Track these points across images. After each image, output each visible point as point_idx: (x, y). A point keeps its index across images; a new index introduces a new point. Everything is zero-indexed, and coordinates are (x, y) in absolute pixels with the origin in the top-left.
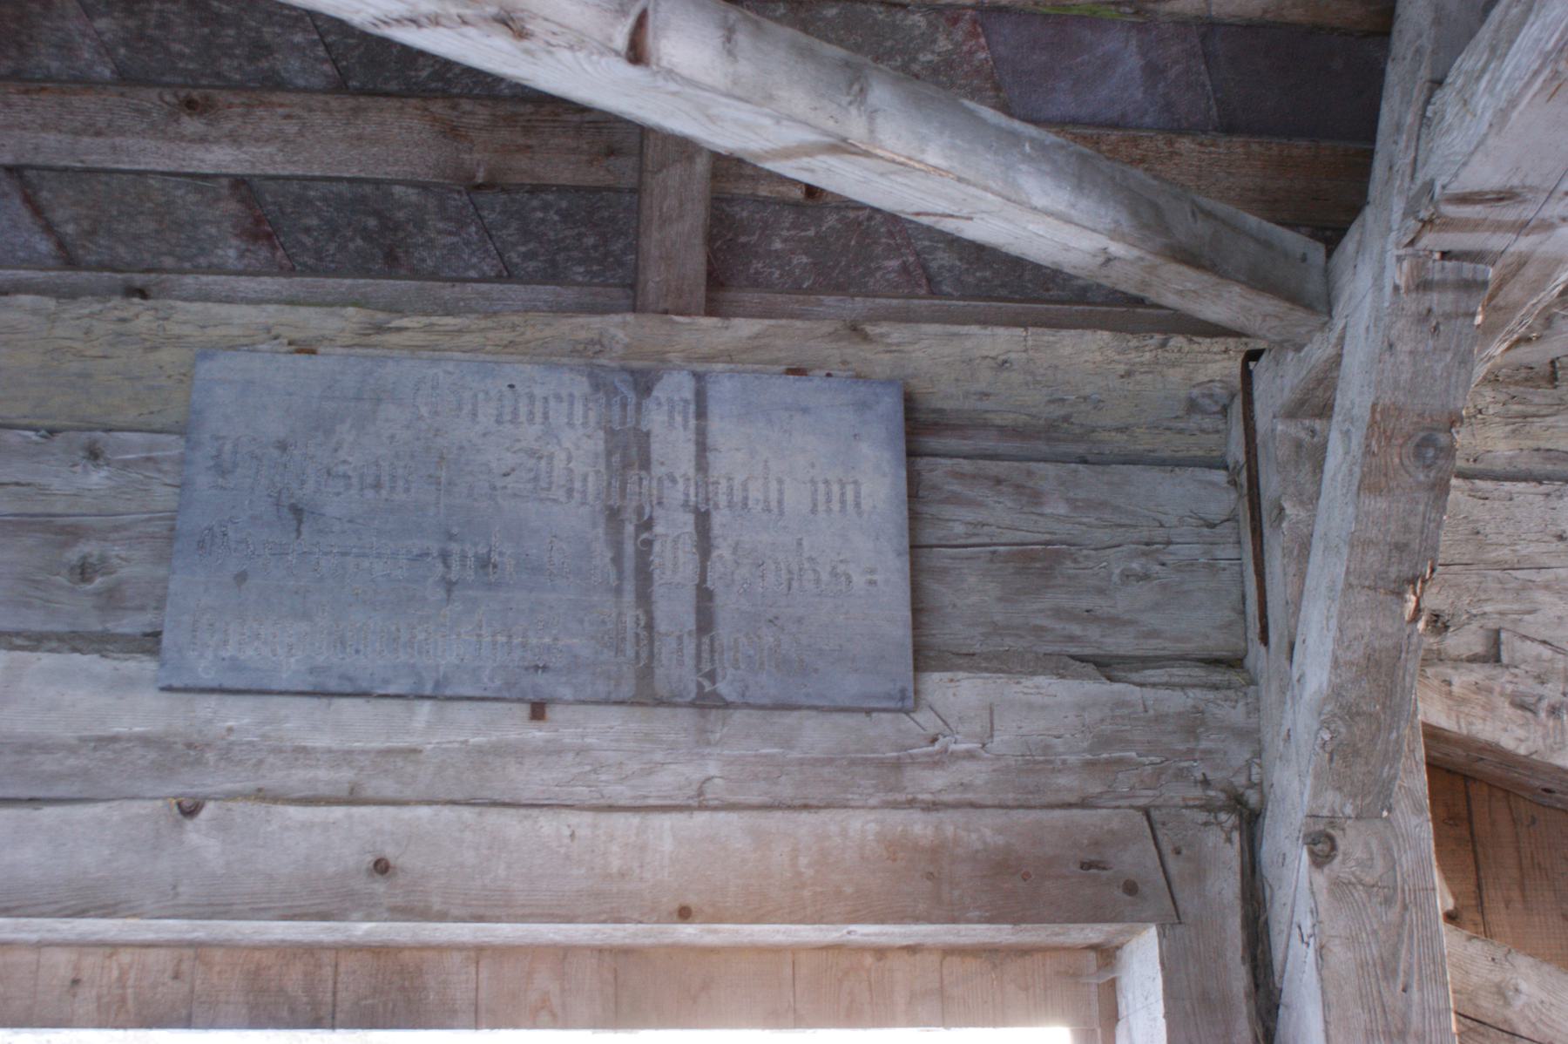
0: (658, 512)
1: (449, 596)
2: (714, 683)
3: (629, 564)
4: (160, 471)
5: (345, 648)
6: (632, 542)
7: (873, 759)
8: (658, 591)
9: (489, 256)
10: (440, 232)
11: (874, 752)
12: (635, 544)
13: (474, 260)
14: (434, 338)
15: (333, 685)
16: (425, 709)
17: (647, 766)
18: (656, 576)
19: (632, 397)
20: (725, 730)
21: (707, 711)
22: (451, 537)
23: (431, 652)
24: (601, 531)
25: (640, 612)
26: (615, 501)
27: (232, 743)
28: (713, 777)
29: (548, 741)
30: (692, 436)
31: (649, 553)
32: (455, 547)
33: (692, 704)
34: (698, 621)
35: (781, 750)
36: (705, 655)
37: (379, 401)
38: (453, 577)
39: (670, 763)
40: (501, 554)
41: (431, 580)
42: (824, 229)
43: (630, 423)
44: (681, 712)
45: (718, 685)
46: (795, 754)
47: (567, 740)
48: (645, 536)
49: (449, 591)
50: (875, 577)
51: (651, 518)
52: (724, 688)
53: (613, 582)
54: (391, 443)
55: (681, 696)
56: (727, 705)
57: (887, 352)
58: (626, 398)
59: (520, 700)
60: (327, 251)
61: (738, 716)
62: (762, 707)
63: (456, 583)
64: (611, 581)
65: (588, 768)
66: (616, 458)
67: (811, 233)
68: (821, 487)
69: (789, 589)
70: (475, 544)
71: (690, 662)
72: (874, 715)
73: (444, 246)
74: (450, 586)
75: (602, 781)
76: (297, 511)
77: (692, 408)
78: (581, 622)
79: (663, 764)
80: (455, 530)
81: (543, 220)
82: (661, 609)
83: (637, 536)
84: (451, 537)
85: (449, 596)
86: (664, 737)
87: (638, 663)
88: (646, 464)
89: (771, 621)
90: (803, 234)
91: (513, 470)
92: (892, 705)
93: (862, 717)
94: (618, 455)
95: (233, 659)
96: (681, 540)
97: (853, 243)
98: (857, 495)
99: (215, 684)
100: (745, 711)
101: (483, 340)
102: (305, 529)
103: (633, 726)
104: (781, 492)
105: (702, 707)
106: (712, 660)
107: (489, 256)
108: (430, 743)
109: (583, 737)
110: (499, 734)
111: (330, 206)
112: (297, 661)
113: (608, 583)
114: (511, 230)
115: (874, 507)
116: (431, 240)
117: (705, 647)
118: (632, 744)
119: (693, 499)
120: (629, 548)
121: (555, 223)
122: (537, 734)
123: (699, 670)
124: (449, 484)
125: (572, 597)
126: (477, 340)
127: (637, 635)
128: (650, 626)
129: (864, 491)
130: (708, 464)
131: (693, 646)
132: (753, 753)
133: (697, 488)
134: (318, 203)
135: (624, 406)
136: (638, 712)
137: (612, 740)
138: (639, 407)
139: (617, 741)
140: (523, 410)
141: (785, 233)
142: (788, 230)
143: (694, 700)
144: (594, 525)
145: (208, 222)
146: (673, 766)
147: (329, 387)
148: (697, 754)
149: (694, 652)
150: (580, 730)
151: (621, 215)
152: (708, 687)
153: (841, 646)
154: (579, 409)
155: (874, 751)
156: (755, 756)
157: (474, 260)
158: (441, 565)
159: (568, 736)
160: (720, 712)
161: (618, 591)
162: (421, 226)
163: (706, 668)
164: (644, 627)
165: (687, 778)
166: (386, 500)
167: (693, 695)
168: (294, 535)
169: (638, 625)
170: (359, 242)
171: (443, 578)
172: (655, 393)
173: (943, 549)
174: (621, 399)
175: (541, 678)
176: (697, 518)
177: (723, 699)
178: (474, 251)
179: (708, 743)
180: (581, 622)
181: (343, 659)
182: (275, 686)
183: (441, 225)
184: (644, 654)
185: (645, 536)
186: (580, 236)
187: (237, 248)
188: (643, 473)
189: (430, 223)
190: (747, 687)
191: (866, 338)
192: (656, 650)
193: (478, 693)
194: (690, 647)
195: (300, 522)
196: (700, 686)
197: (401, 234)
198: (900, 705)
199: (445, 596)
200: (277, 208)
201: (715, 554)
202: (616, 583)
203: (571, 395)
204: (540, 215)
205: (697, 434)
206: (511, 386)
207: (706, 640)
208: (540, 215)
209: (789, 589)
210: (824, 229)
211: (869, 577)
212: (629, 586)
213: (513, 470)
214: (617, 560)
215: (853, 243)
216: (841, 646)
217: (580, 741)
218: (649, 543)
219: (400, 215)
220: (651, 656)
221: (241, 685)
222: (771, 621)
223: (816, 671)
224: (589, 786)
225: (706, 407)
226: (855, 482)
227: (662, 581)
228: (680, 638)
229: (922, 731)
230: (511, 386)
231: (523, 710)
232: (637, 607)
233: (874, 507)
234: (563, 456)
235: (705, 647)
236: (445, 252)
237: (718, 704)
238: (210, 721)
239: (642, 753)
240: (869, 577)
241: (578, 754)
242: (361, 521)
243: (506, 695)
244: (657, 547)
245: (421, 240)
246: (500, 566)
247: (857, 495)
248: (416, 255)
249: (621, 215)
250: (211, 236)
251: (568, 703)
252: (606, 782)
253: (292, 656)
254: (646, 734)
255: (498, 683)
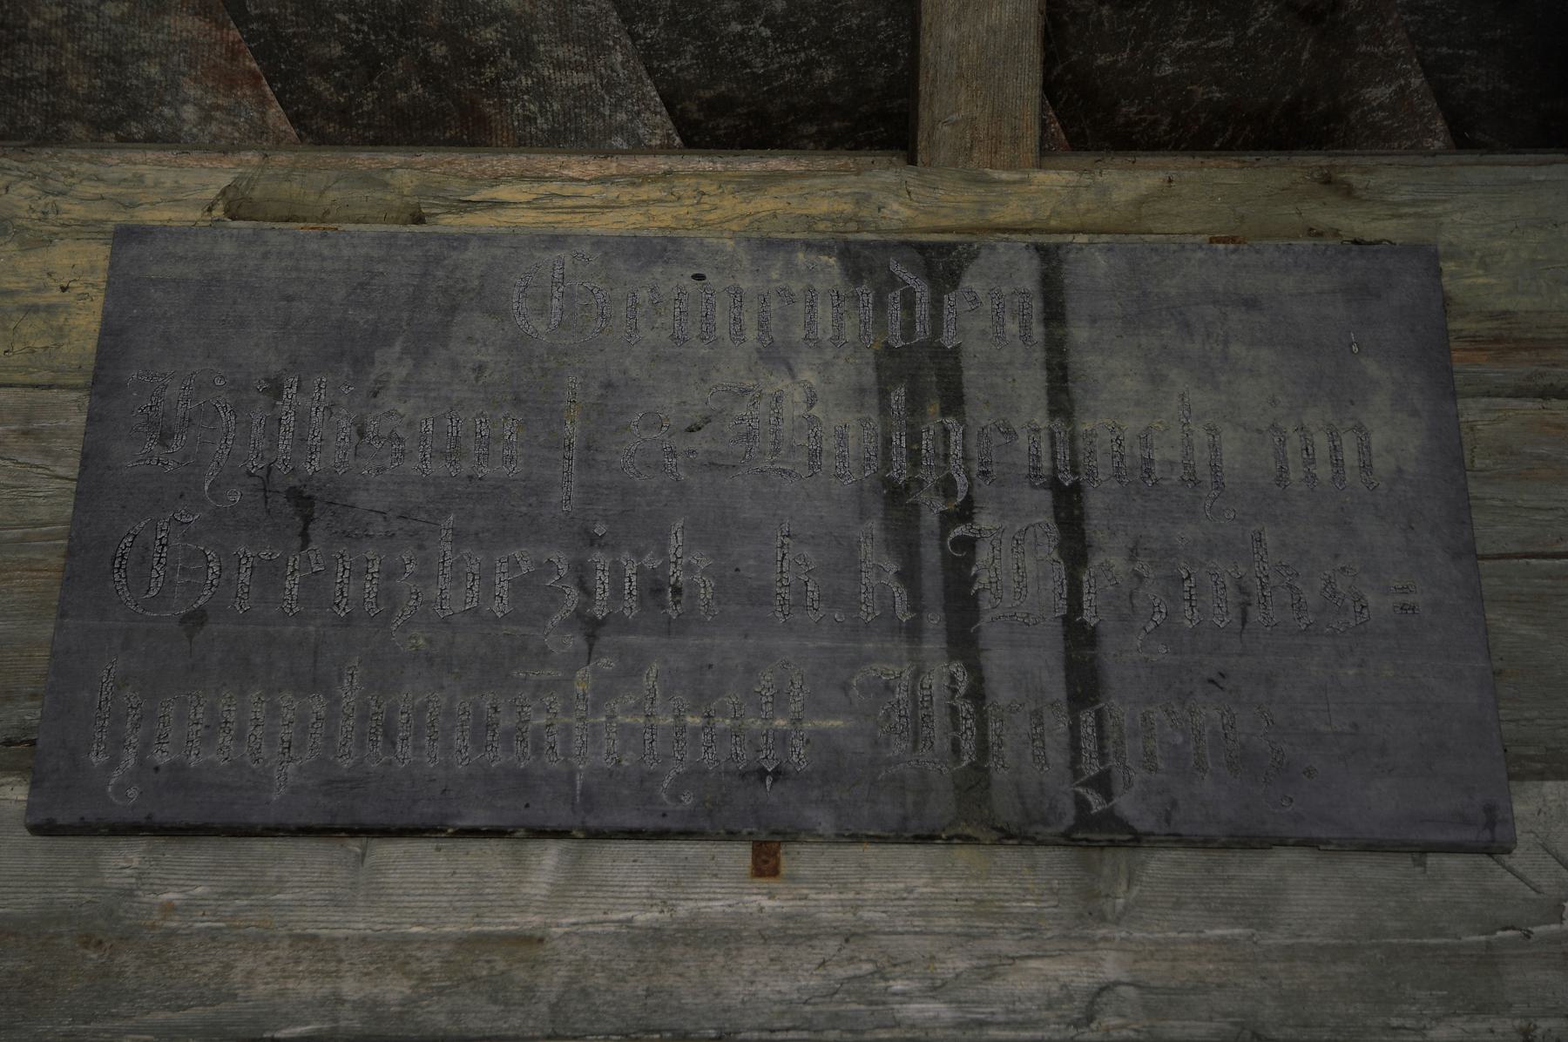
0: (983, 489)
1: (591, 646)
2: (1108, 795)
3: (932, 583)
4: (47, 452)
5: (394, 744)
6: (936, 543)
7: (1437, 947)
8: (990, 629)
9: (648, 108)
10: (559, 65)
11: (1436, 935)
12: (943, 547)
13: (622, 116)
14: (550, 218)
15: (369, 815)
16: (549, 858)
17: (983, 963)
18: (985, 605)
19: (922, 291)
20: (1135, 891)
21: (1095, 855)
22: (593, 541)
23: (558, 748)
24: (874, 525)
25: (957, 668)
26: (900, 470)
27: (173, 933)
28: (1117, 983)
29: (788, 917)
30: (1039, 355)
31: (970, 561)
32: (600, 558)
33: (1068, 839)
34: (1070, 683)
35: (1249, 931)
36: (1089, 746)
37: (454, 309)
38: (599, 611)
39: (1029, 957)
40: (689, 568)
41: (556, 619)
42: (1251, 32)
43: (922, 331)
44: (1043, 855)
45: (1115, 800)
46: (1278, 938)
47: (826, 916)
48: (960, 530)
49: (591, 638)
50: (1410, 599)
51: (969, 500)
52: (1126, 805)
53: (904, 615)
54: (477, 379)
55: (1046, 823)
56: (1137, 840)
57: (1394, 216)
58: (912, 291)
59: (732, 836)
60: (360, 105)
61: (1160, 865)
62: (1206, 844)
63: (602, 623)
64: (899, 614)
65: (867, 967)
66: (898, 396)
67: (1228, 41)
68: (1295, 441)
69: (1244, 621)
70: (639, 554)
71: (1058, 757)
72: (1432, 860)
73: (568, 90)
74: (592, 628)
75: (895, 994)
76: (303, 501)
77: (1037, 305)
78: (845, 688)
79: (1013, 958)
80: (600, 529)
81: (742, 37)
82: (997, 660)
83: (943, 535)
84: (593, 541)
85: (591, 646)
86: (1014, 907)
87: (959, 760)
88: (954, 401)
89: (1211, 681)
90: (1212, 44)
91: (707, 420)
92: (1468, 835)
93: (1403, 863)
94: (906, 213)
95: (177, 768)
96: (1030, 537)
97: (1305, 56)
98: (1364, 449)
99: (139, 816)
100: (1173, 855)
101: (642, 219)
102: (317, 531)
103: (951, 886)
104: (1214, 447)
105: (1090, 844)
106: (1103, 757)
107: (648, 108)
108: (558, 926)
109: (856, 908)
110: (691, 904)
111: (362, 21)
112: (300, 768)
113: (894, 616)
114: (687, 60)
115: (1400, 470)
116: (542, 81)
117: (1088, 730)
118: (952, 921)
119: (1046, 463)
120: (931, 555)
121: (764, 43)
122: (763, 901)
123: (1077, 774)
124: (588, 448)
125: (826, 644)
126: (632, 220)
127: (954, 711)
128: (977, 694)
129: (1377, 440)
130: (1071, 401)
131: (1063, 727)
132: (1194, 935)
133: (1053, 444)
134: (342, 17)
135: (909, 304)
136: (963, 855)
137: (912, 914)
138: (936, 304)
139: (924, 914)
140: (721, 318)
141: (1180, 44)
142: (1186, 37)
143: (1073, 829)
144: (863, 515)
145: (144, 54)
146: (1033, 964)
147: (362, 285)
148: (1082, 938)
149: (1065, 740)
150: (851, 895)
151: (883, 23)
152: (1096, 803)
153: (1355, 726)
154: (825, 314)
155: (1438, 932)
156: (1198, 942)
157: (622, 116)
158: (575, 592)
159: (826, 905)
160: (1122, 855)
161: (913, 632)
162: (525, 53)
163: (1092, 769)
164: (966, 696)
165: (1064, 986)
166: (470, 477)
167: (1069, 820)
168: (297, 543)
169: (955, 691)
170: (417, 89)
171: (579, 614)
172: (967, 282)
173: (1533, 561)
174: (903, 294)
175: (770, 792)
176: (1056, 497)
177: (1131, 830)
178: (620, 99)
179: (1103, 919)
180: (845, 688)
181: (390, 763)
182: (256, 819)
183: (561, 52)
184: (968, 746)
185: (960, 530)
186: (811, 64)
187: (197, 103)
188: (950, 421)
189: (542, 48)
190: (1174, 804)
191: (1348, 192)
192: (992, 738)
193: (651, 823)
194: (1059, 726)
195: (308, 520)
196: (1081, 804)
197: (489, 72)
198: (1486, 835)
199: (585, 647)
200: (266, 27)
201: (1096, 561)
202: (909, 616)
203: (810, 289)
204: (736, 27)
205: (1049, 350)
206: (699, 277)
207: (1087, 717)
208: (736, 27)
209: (1244, 621)
210: (1251, 32)
211: (1400, 598)
212: (934, 620)
213: (707, 420)
214: (909, 576)
215: (1305, 56)
216: (1355, 726)
217: (849, 916)
218: (968, 544)
219: (489, 35)
220: (983, 749)
221: (190, 817)
222: (1211, 681)
223: (1309, 772)
224: (871, 1003)
225: (1062, 305)
226: (1359, 428)
227: (998, 612)
228: (1037, 715)
229: (1532, 894)
230: (699, 277)
231: (739, 855)
232: (952, 658)
233: (1400, 470)
234: (799, 396)
235: (1088, 730)
236: (569, 102)
237: (1119, 837)
238: (129, 893)
239: (970, 937)
240: (1400, 598)
241: (847, 941)
242: (424, 516)
243: (706, 825)
244: (984, 554)
245: (526, 82)
246: (686, 592)
247: (1364, 449)
248: (518, 109)
249: (883, 23)
250: (149, 82)
251: (822, 839)
252: (904, 994)
253: (292, 760)
254: (980, 902)
255: (688, 800)
